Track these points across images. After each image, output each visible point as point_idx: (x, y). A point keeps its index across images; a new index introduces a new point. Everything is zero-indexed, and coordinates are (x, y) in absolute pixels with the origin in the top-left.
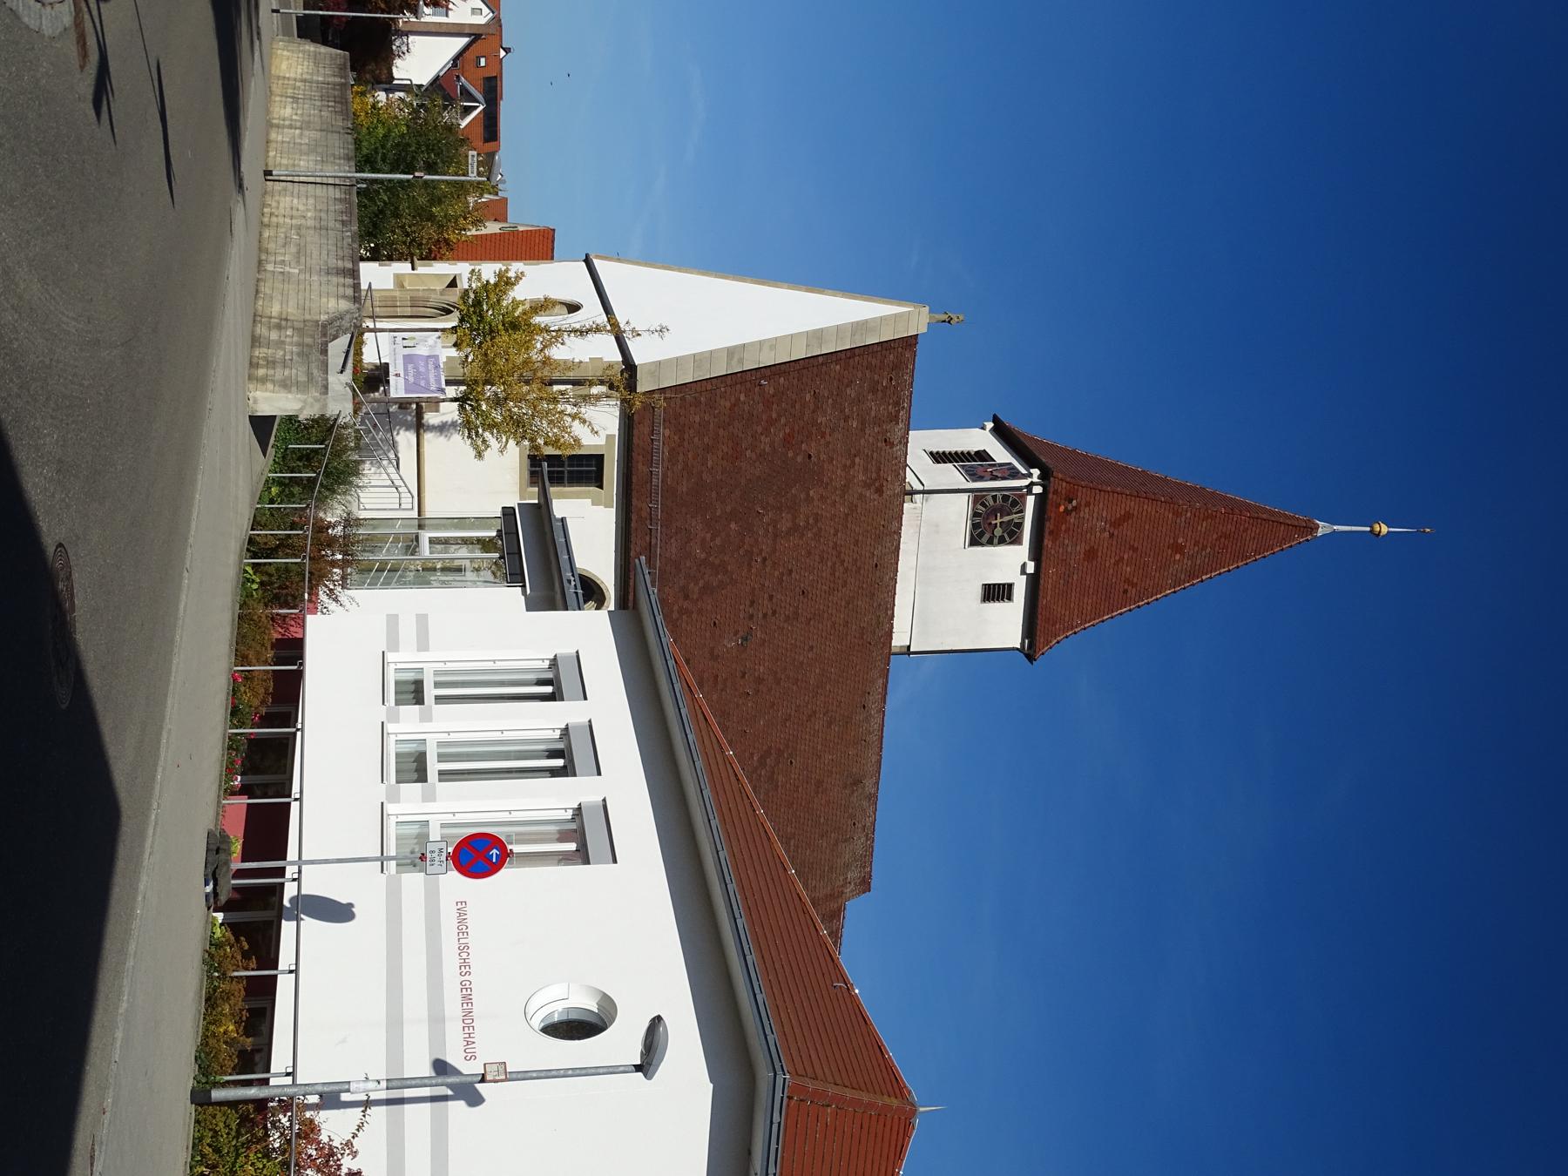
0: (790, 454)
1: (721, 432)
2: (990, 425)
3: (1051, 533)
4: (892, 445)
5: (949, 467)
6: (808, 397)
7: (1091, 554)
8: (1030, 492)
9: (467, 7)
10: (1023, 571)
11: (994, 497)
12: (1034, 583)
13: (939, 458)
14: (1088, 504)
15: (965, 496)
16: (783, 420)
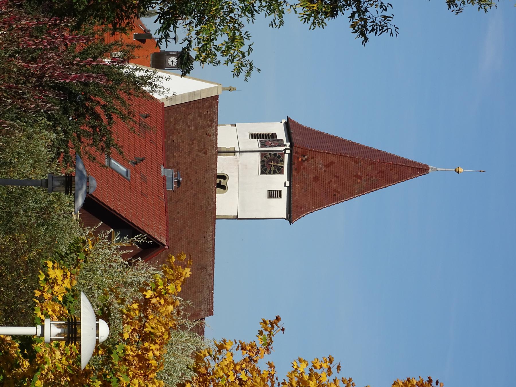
2: (284, 121)
3: (296, 169)
4: (210, 136)
7: (316, 179)
8: (285, 153)
9: (0, 214)
10: (285, 186)
11: (270, 154)
12: (289, 189)
14: (313, 158)
15: (257, 154)
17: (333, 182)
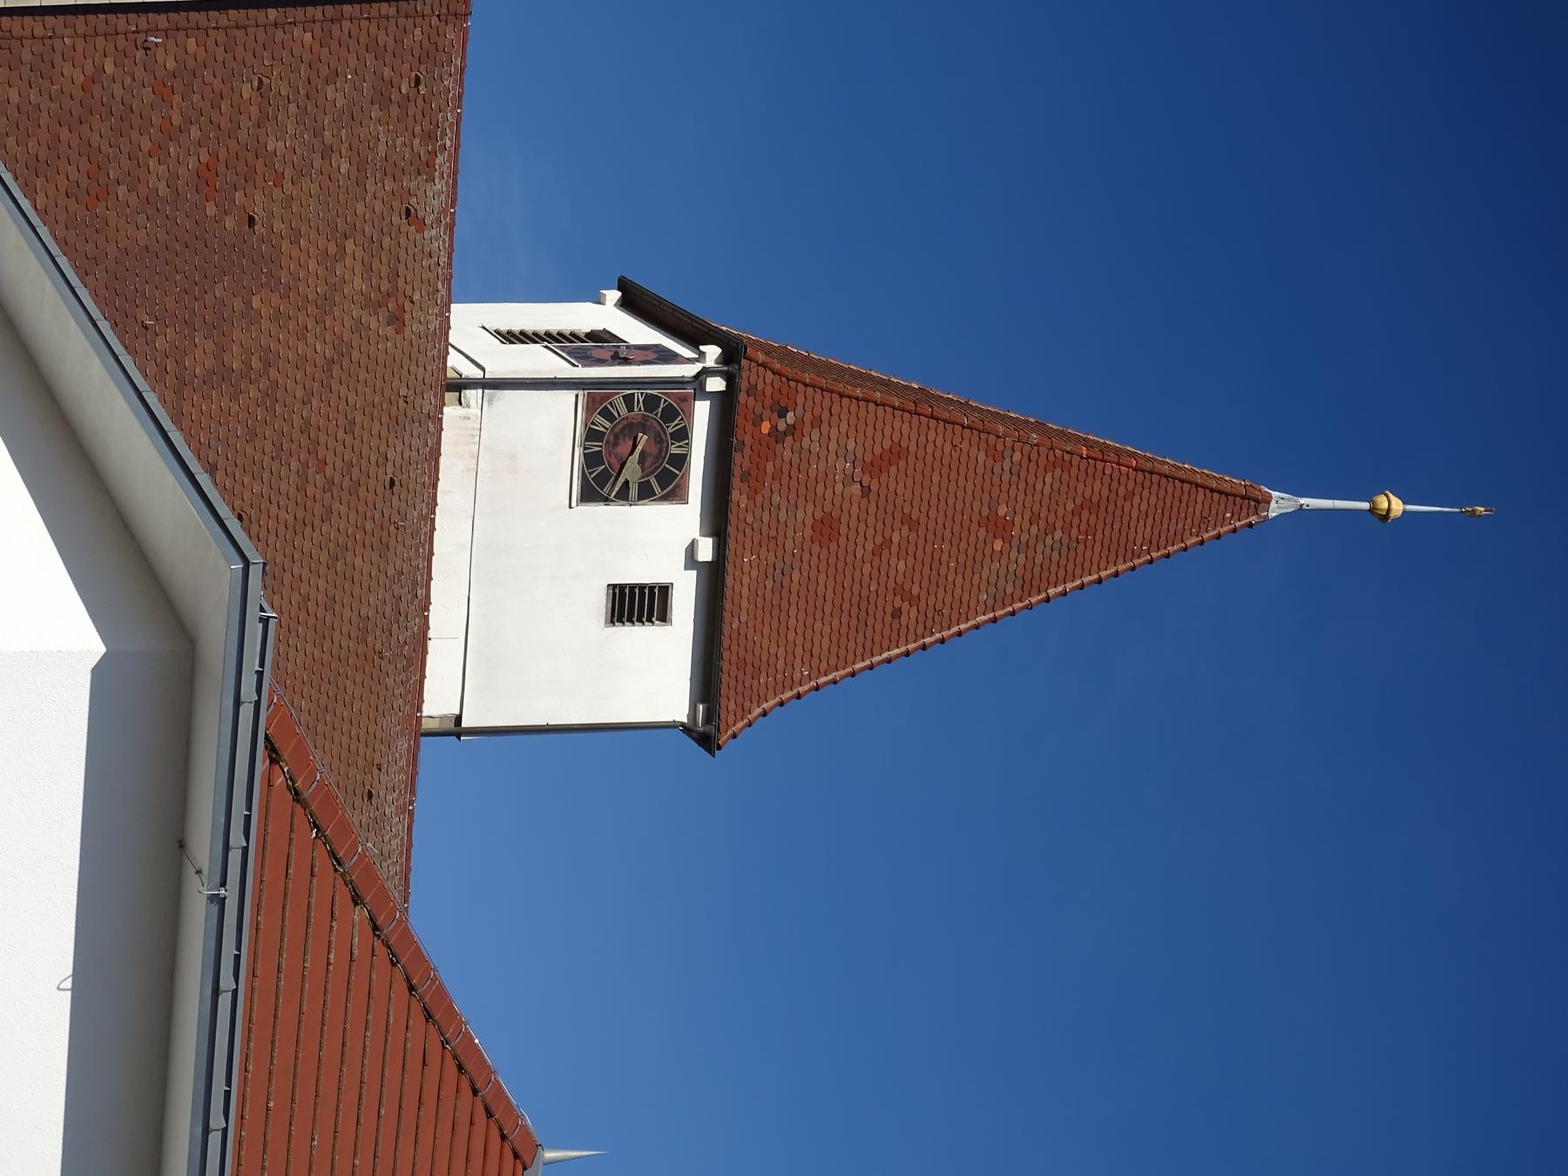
0: (211, 210)
1: (64, 134)
2: (613, 295)
5: (537, 349)
6: (246, 91)
7: (826, 529)
11: (629, 400)
12: (713, 580)
13: (509, 337)
14: (817, 422)
15: (568, 397)
16: (195, 133)
17: (894, 548)
